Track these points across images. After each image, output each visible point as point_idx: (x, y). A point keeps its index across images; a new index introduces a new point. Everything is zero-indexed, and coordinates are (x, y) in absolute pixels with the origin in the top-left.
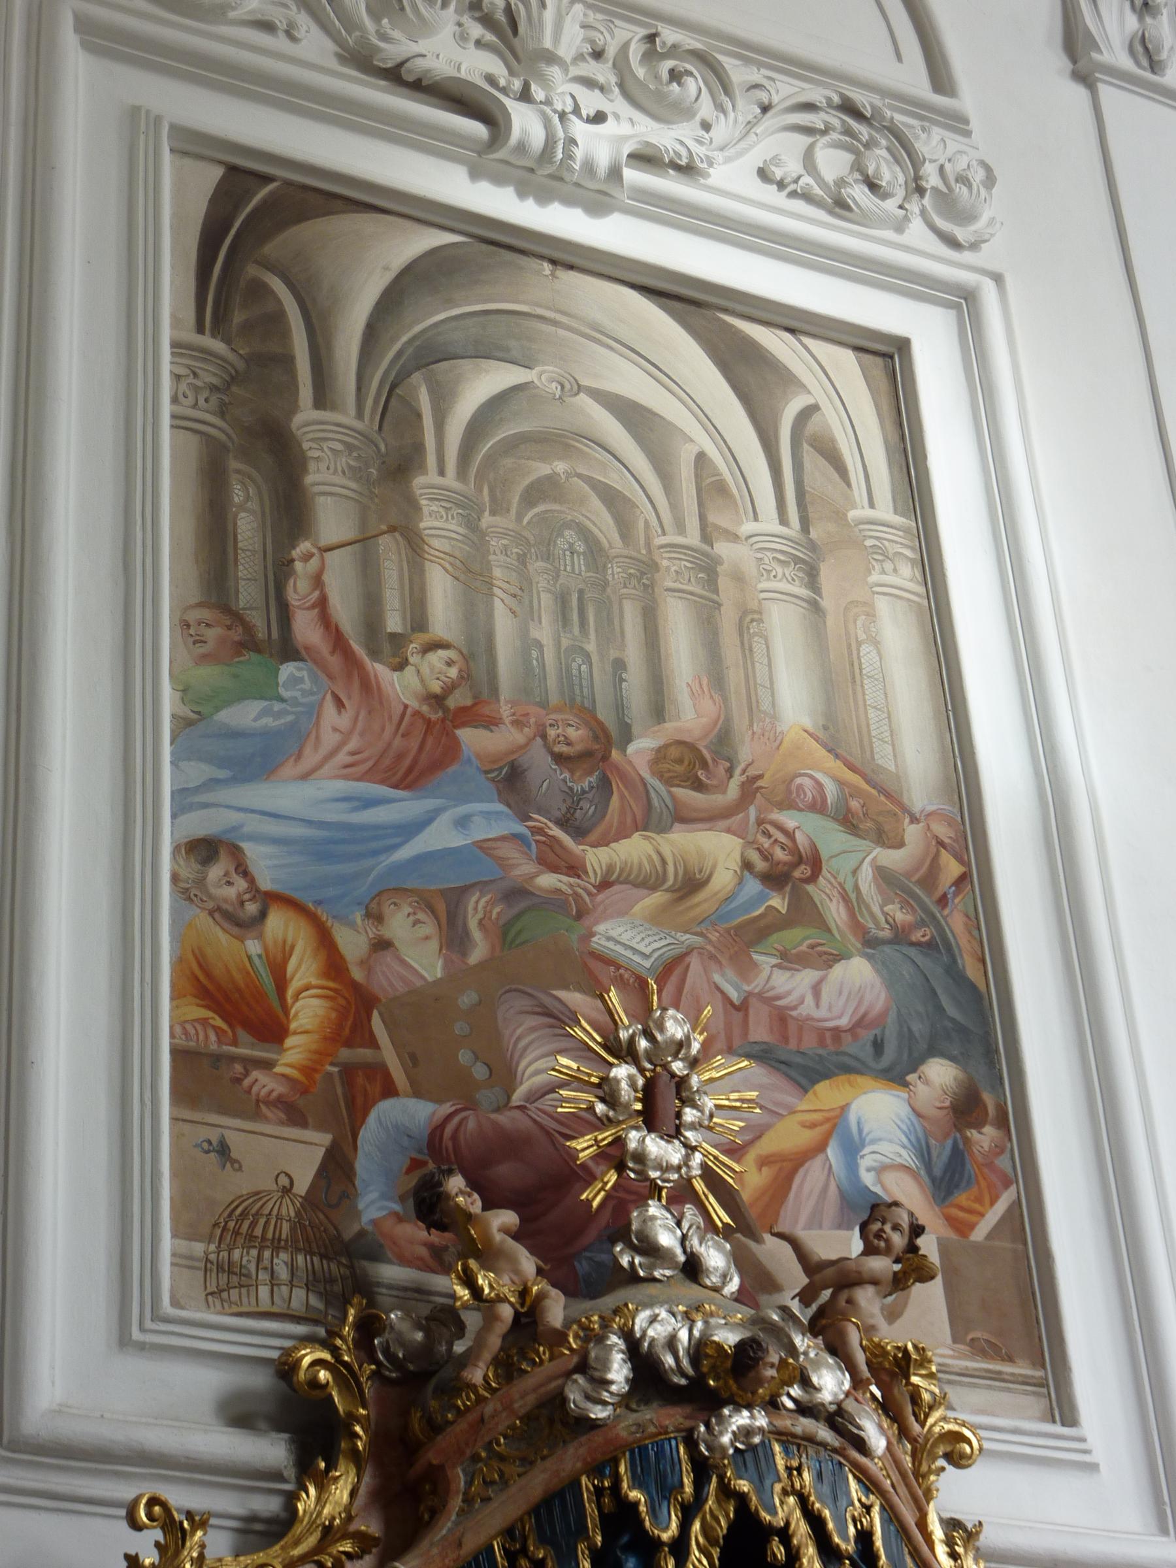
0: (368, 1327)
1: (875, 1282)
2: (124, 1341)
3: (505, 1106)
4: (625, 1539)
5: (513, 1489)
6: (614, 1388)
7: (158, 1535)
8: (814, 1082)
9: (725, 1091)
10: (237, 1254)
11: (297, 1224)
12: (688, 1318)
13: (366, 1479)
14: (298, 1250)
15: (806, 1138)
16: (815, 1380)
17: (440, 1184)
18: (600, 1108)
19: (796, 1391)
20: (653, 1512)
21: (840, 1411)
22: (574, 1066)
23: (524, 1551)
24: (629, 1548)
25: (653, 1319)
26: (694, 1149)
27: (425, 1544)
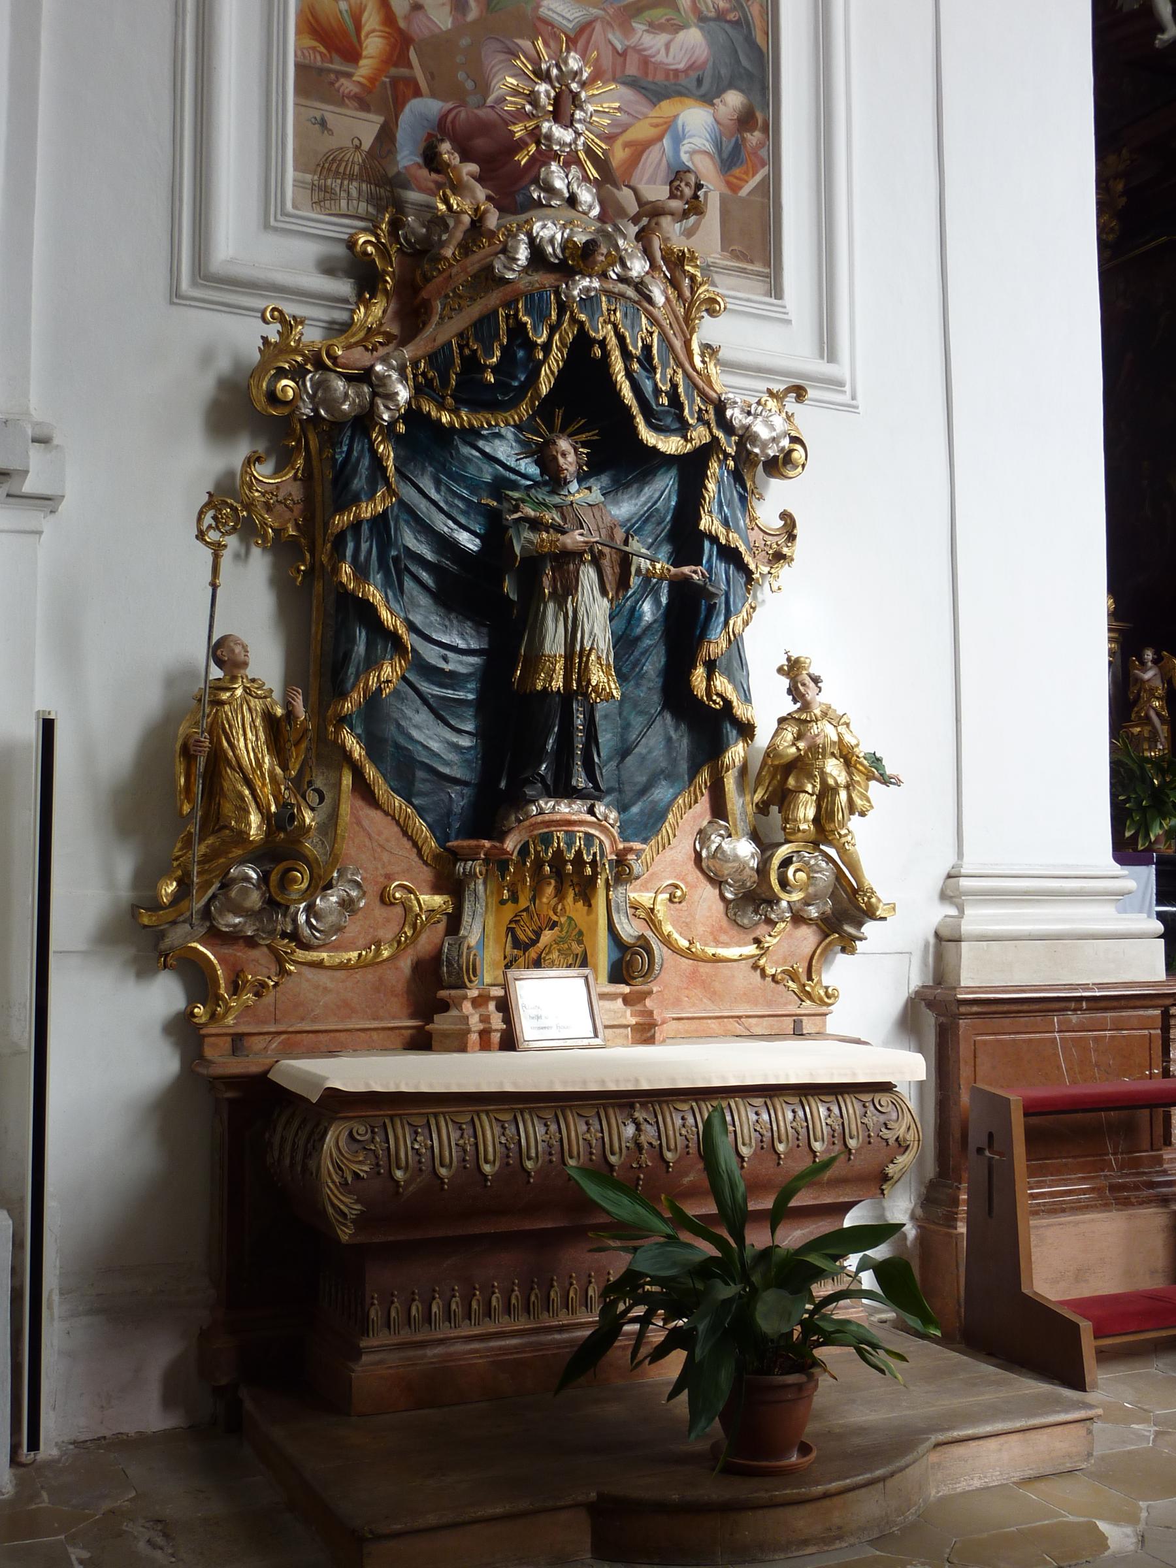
0: (395, 224)
1: (672, 214)
2: (267, 226)
3: (483, 105)
4: (519, 341)
5: (463, 314)
6: (519, 263)
7: (278, 327)
8: (660, 101)
9: (603, 104)
10: (329, 181)
11: (363, 167)
12: (564, 227)
13: (392, 305)
14: (363, 181)
15: (651, 132)
16: (629, 264)
17: (436, 147)
18: (528, 107)
19: (618, 269)
20: (535, 328)
21: (642, 282)
22: (515, 83)
23: (467, 345)
24: (520, 346)
25: (544, 227)
26: (580, 134)
27: (418, 338)
